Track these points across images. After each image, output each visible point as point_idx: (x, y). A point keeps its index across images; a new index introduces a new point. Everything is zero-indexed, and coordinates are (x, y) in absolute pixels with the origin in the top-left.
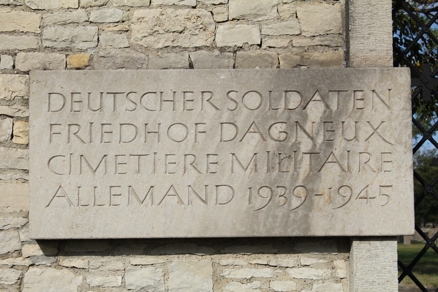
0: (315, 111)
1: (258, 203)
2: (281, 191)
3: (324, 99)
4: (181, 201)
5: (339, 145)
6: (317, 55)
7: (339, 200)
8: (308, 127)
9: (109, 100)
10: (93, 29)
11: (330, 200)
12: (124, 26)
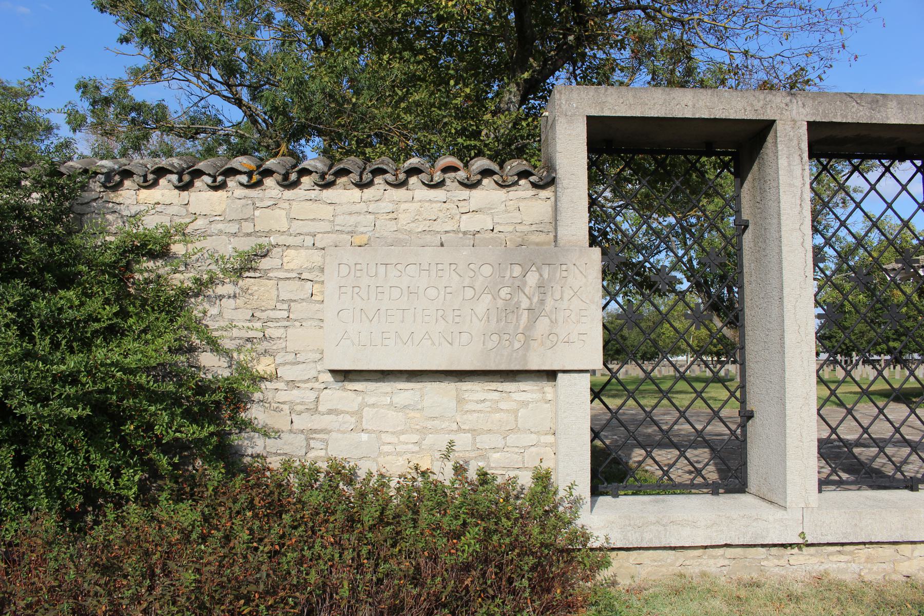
0: (532, 279)
1: (490, 345)
2: (507, 337)
3: (538, 270)
4: (433, 344)
5: (549, 304)
9: (382, 269)
10: (371, 217)
11: (542, 344)
12: (394, 215)
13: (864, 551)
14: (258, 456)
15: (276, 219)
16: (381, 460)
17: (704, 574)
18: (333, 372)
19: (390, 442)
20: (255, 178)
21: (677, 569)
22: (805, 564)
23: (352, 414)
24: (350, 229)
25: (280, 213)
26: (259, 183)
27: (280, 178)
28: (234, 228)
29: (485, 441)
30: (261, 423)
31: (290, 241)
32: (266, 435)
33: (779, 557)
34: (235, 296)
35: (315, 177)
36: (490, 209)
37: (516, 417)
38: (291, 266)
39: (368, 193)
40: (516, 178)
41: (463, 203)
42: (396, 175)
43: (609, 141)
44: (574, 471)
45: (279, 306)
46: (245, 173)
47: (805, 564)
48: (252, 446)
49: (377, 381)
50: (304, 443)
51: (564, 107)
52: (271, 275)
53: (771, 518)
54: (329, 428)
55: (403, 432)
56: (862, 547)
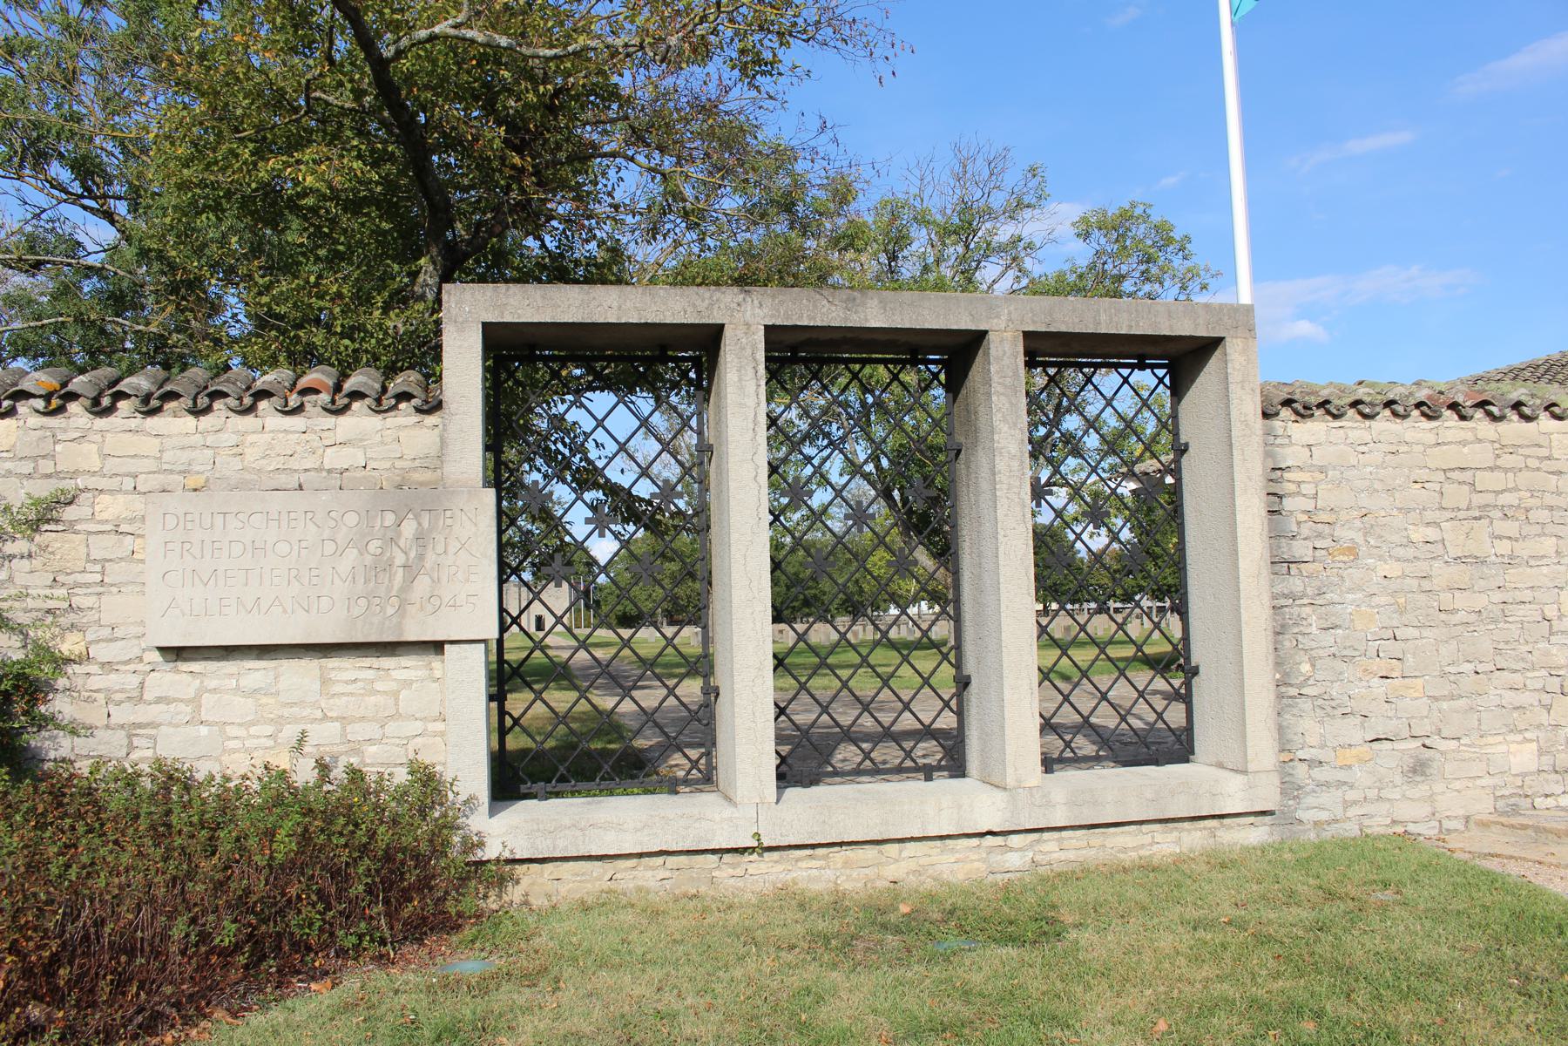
0: (409, 528)
1: (356, 611)
2: (377, 601)
3: (416, 517)
4: (285, 611)
5: (430, 558)
6: (417, 476)
7: (430, 608)
8: (402, 543)
9: (219, 519)
10: (210, 452)
11: (422, 608)
12: (239, 450)
13: (839, 855)
14: (64, 760)
15: (86, 456)
16: (225, 759)
17: (639, 889)
18: (160, 649)
19: (236, 735)
20: (55, 402)
21: (606, 885)
22: (766, 873)
23: (187, 702)
24: (182, 468)
25: (90, 449)
26: (61, 410)
27: (88, 403)
28: (27, 467)
29: (358, 731)
30: (68, 717)
31: (103, 483)
32: (74, 732)
33: (734, 866)
34: (30, 556)
35: (134, 402)
36: (362, 440)
37: (397, 700)
38: (105, 516)
39: (205, 421)
40: (393, 402)
41: (326, 434)
42: (240, 399)
43: (507, 350)
44: (467, 769)
45: (90, 567)
46: (40, 396)
47: (766, 873)
48: (54, 747)
49: (218, 659)
50: (125, 742)
51: (454, 312)
52: (78, 527)
53: (717, 817)
54: (158, 720)
55: (253, 723)
56: (837, 849)
